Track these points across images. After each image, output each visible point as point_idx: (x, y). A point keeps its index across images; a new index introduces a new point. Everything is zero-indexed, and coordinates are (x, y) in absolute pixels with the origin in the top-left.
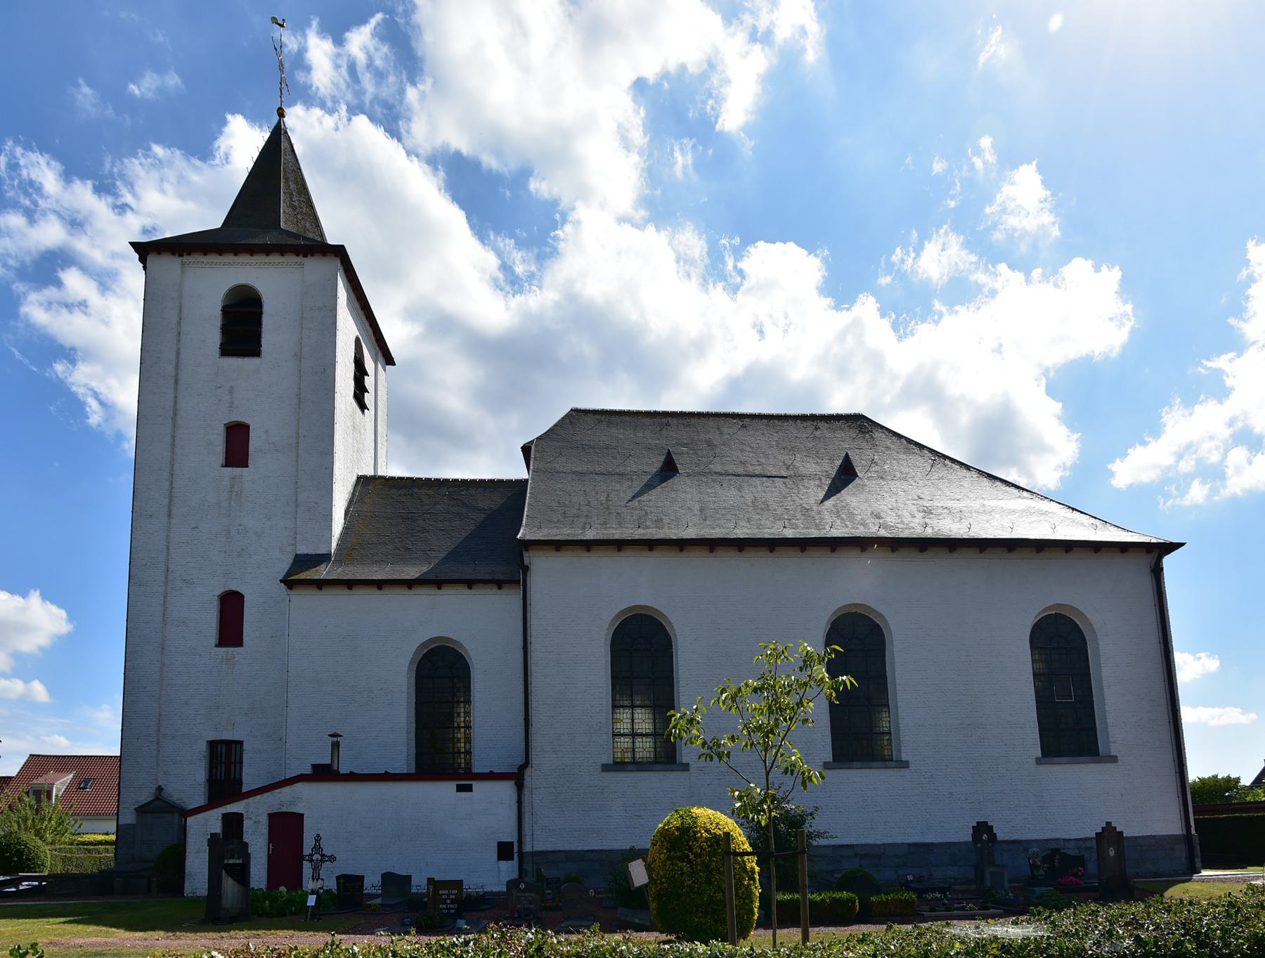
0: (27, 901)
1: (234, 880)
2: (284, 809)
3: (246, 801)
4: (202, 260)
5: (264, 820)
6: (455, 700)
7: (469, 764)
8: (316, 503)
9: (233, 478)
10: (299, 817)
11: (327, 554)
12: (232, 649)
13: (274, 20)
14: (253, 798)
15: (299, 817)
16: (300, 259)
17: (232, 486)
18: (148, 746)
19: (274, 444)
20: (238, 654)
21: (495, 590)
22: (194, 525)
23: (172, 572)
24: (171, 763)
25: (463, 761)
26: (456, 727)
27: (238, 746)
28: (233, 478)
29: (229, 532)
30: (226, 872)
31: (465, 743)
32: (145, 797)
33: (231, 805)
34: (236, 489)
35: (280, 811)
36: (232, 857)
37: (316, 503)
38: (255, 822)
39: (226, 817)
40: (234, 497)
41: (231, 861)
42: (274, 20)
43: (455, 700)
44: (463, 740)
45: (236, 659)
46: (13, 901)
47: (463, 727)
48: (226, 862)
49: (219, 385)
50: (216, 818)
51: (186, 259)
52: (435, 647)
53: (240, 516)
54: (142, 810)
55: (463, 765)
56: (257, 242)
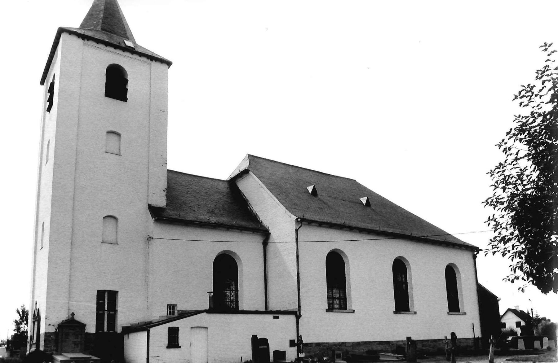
44: (234, 296)
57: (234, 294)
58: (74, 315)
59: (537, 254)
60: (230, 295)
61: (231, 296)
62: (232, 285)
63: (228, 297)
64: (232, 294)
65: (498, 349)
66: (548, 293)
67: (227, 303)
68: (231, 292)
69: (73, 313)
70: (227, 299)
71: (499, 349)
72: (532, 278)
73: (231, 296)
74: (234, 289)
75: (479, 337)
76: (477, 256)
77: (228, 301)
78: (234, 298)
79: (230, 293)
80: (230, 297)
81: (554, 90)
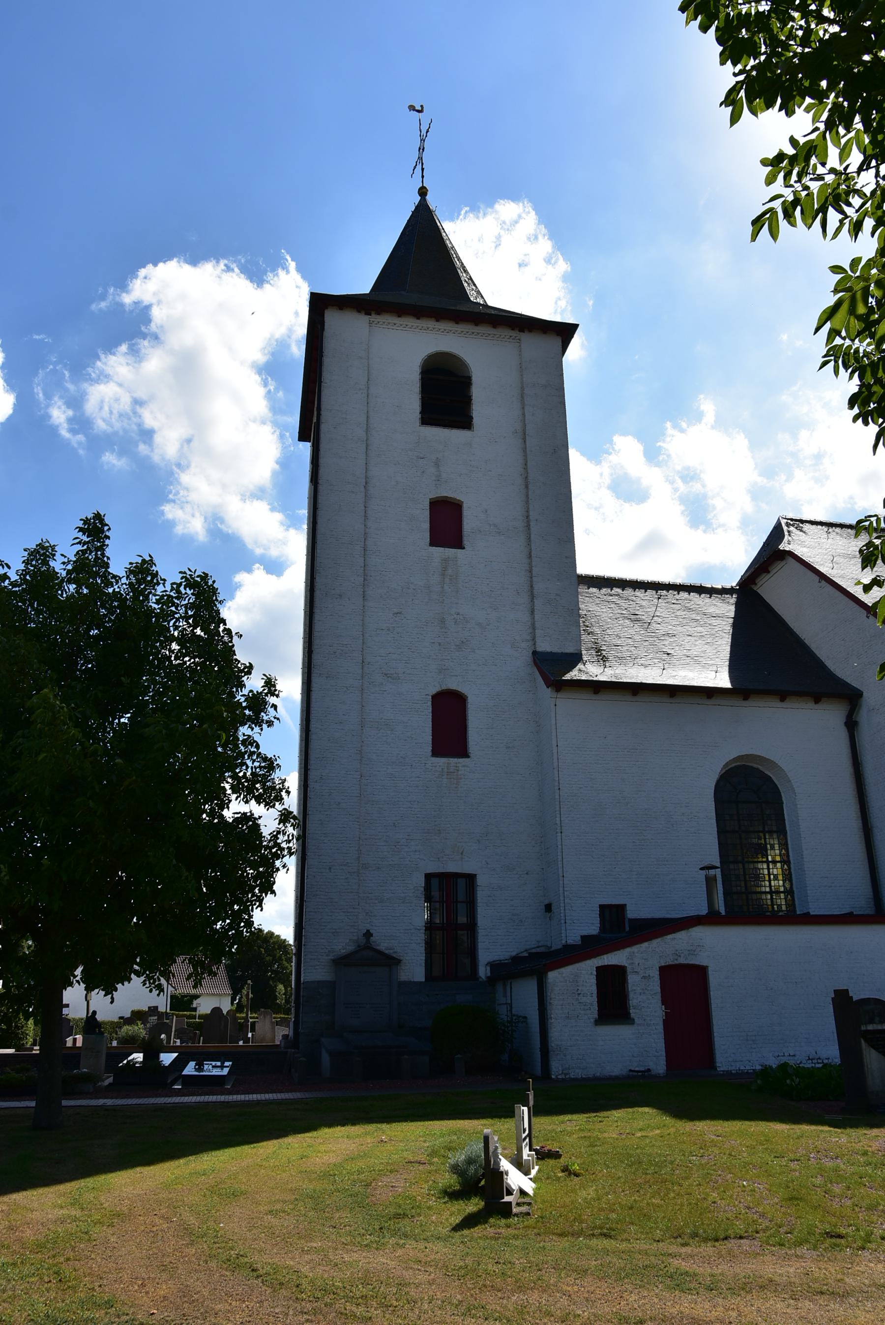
0: (193, 1095)
1: (879, 1052)
2: (682, 961)
3: (628, 950)
4: (395, 322)
5: (655, 974)
6: (767, 829)
7: (791, 905)
8: (557, 595)
9: (446, 560)
10: (702, 971)
11: (576, 654)
12: (456, 760)
13: (412, 108)
14: (638, 946)
15: (702, 971)
16: (515, 333)
17: (445, 569)
18: (347, 879)
19: (495, 525)
20: (464, 766)
21: (811, 705)
22: (396, 610)
23: (369, 663)
24: (376, 902)
25: (783, 902)
26: (771, 862)
27: (461, 882)
28: (446, 560)
29: (442, 621)
30: (866, 1041)
31: (784, 881)
32: (343, 945)
33: (609, 955)
34: (450, 572)
35: (676, 962)
36: (872, 1021)
37: (557, 595)
38: (644, 977)
39: (603, 973)
40: (447, 580)
41: (870, 1027)
42: (412, 108)
43: (767, 829)
44: (780, 877)
45: (460, 773)
46: (128, 1096)
47: (778, 862)
48: (863, 1028)
49: (422, 456)
50: (589, 972)
51: (374, 318)
52: (735, 766)
53: (456, 603)
54: (341, 962)
55: (784, 908)
56: (465, 309)
57: (780, 871)
58: (372, 935)
59: (137, 958)
60: (769, 875)
61: (772, 877)
62: (773, 848)
63: (764, 881)
64: (775, 872)
65: (246, 818)
66: (851, 994)
67: (764, 897)
68: (771, 867)
69: (368, 931)
70: (761, 886)
71: (860, 100)
72: (191, 1063)
73: (772, 877)
74: (778, 859)
75: (120, 984)
76: (85, 990)
77: (766, 893)
78: (781, 883)
79: (768, 869)
80: (770, 881)
81: (260, 764)
